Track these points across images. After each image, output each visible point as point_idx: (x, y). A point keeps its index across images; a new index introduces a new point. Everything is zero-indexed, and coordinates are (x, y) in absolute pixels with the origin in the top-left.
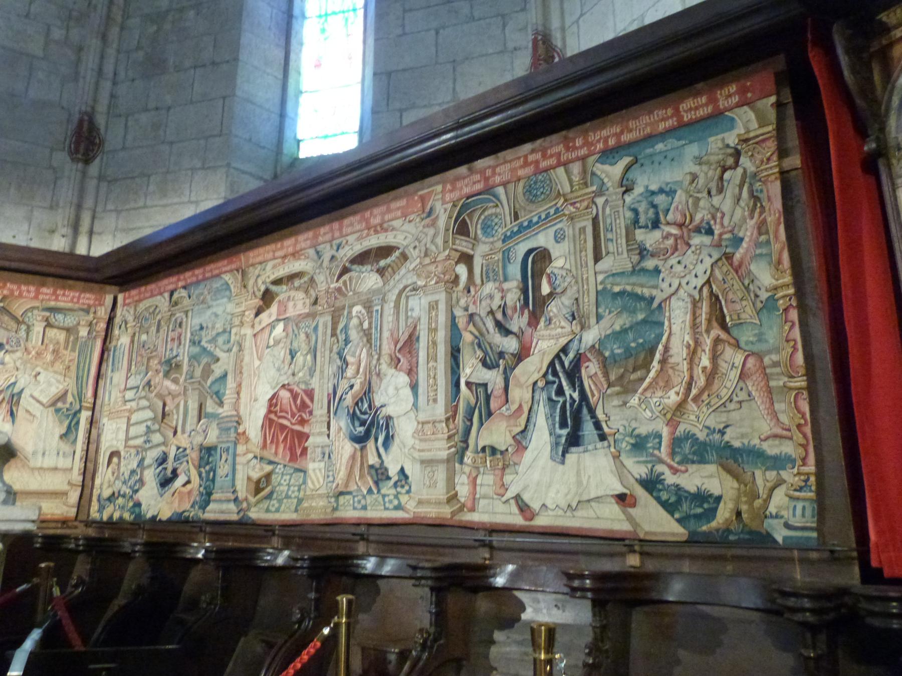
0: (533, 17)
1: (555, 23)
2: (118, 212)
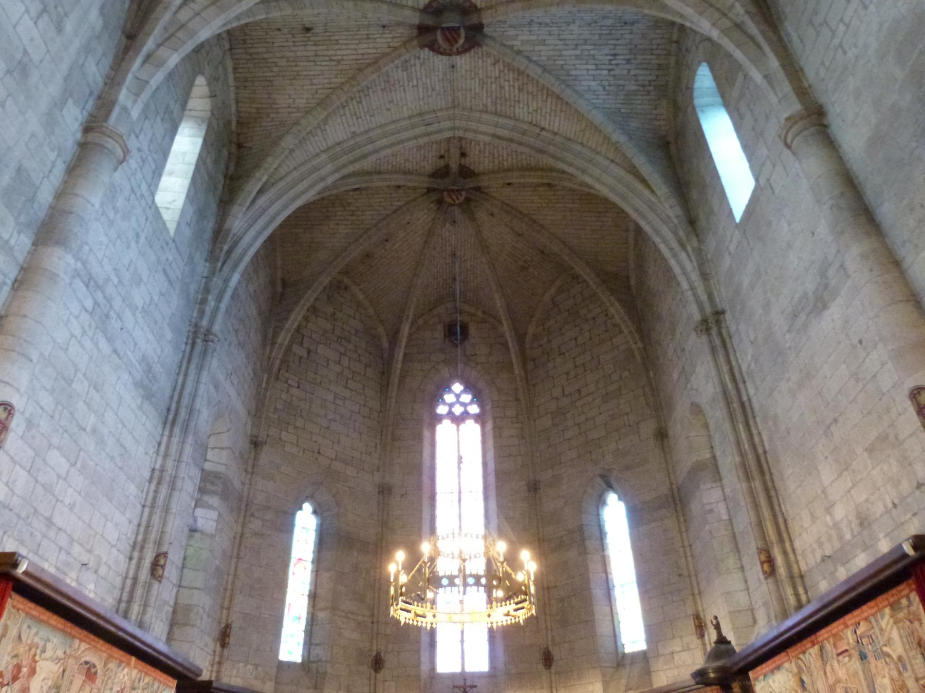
0: (690, 611)
1: (700, 609)
2: (565, 687)
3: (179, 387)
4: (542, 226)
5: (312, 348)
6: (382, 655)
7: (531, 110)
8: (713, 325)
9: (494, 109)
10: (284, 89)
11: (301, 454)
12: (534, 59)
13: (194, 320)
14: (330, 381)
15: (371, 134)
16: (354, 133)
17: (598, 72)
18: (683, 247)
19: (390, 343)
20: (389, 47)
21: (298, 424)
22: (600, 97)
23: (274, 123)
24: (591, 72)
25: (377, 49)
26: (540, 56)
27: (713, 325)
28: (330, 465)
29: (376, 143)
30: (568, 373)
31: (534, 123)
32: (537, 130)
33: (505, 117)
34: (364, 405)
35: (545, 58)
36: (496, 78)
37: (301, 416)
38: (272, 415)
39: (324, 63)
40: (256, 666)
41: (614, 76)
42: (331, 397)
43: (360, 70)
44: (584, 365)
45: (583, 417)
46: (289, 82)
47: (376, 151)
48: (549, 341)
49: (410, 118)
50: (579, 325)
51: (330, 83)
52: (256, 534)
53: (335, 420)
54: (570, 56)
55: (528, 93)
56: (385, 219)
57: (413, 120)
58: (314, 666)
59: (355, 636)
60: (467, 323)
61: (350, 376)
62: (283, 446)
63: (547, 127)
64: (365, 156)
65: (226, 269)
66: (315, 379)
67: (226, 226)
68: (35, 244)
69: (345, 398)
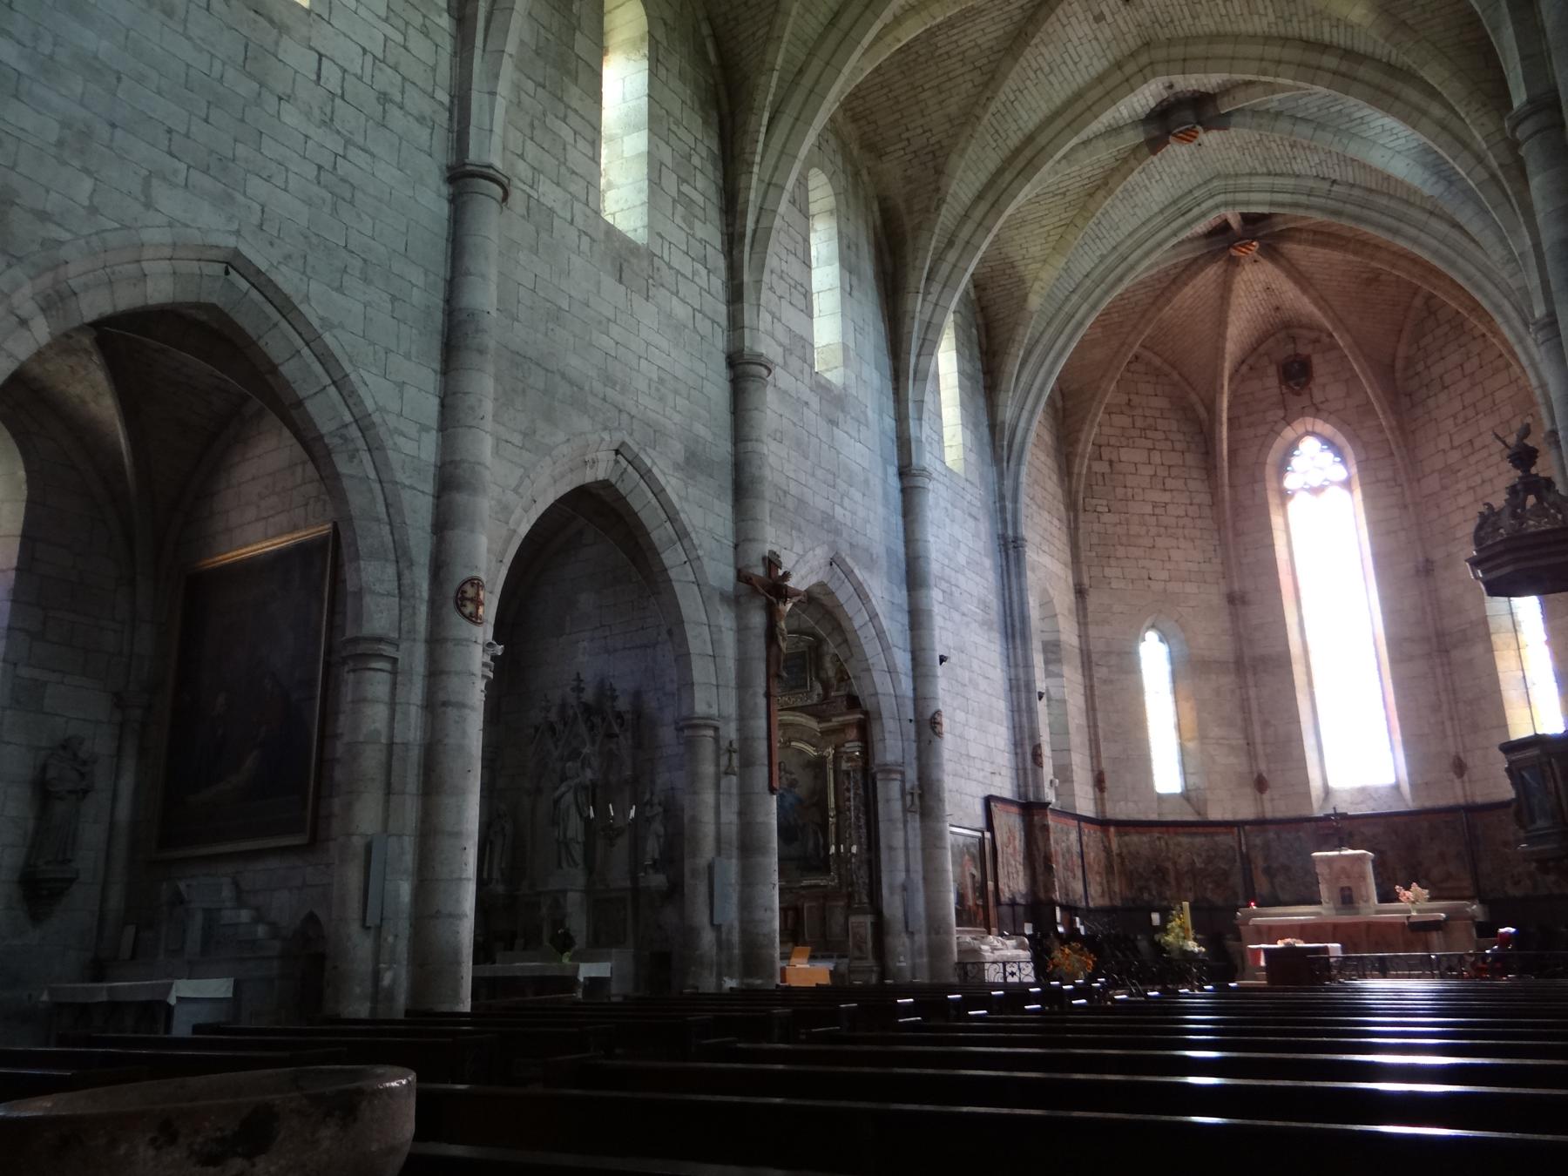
3: (1007, 601)
5: (1114, 458)
6: (1265, 775)
10: (1013, 240)
11: (1130, 586)
13: (1000, 532)
14: (1143, 489)
20: (1117, 160)
21: (1118, 555)
22: (1400, 135)
25: (1103, 167)
26: (1307, 109)
28: (1165, 590)
33: (1282, 175)
34: (1191, 504)
36: (1258, 142)
37: (1122, 545)
38: (1089, 554)
39: (1047, 201)
42: (1148, 509)
43: (1091, 195)
44: (1474, 405)
45: (1478, 479)
46: (1016, 232)
47: (1132, 268)
49: (1161, 211)
50: (1465, 345)
53: (1159, 536)
55: (1304, 149)
58: (1193, 794)
59: (1232, 760)
60: (1309, 357)
62: (1110, 583)
63: (1338, 178)
64: (1120, 279)
65: (1012, 464)
66: (1126, 493)
67: (1000, 418)
68: (909, 590)
69: (1166, 504)
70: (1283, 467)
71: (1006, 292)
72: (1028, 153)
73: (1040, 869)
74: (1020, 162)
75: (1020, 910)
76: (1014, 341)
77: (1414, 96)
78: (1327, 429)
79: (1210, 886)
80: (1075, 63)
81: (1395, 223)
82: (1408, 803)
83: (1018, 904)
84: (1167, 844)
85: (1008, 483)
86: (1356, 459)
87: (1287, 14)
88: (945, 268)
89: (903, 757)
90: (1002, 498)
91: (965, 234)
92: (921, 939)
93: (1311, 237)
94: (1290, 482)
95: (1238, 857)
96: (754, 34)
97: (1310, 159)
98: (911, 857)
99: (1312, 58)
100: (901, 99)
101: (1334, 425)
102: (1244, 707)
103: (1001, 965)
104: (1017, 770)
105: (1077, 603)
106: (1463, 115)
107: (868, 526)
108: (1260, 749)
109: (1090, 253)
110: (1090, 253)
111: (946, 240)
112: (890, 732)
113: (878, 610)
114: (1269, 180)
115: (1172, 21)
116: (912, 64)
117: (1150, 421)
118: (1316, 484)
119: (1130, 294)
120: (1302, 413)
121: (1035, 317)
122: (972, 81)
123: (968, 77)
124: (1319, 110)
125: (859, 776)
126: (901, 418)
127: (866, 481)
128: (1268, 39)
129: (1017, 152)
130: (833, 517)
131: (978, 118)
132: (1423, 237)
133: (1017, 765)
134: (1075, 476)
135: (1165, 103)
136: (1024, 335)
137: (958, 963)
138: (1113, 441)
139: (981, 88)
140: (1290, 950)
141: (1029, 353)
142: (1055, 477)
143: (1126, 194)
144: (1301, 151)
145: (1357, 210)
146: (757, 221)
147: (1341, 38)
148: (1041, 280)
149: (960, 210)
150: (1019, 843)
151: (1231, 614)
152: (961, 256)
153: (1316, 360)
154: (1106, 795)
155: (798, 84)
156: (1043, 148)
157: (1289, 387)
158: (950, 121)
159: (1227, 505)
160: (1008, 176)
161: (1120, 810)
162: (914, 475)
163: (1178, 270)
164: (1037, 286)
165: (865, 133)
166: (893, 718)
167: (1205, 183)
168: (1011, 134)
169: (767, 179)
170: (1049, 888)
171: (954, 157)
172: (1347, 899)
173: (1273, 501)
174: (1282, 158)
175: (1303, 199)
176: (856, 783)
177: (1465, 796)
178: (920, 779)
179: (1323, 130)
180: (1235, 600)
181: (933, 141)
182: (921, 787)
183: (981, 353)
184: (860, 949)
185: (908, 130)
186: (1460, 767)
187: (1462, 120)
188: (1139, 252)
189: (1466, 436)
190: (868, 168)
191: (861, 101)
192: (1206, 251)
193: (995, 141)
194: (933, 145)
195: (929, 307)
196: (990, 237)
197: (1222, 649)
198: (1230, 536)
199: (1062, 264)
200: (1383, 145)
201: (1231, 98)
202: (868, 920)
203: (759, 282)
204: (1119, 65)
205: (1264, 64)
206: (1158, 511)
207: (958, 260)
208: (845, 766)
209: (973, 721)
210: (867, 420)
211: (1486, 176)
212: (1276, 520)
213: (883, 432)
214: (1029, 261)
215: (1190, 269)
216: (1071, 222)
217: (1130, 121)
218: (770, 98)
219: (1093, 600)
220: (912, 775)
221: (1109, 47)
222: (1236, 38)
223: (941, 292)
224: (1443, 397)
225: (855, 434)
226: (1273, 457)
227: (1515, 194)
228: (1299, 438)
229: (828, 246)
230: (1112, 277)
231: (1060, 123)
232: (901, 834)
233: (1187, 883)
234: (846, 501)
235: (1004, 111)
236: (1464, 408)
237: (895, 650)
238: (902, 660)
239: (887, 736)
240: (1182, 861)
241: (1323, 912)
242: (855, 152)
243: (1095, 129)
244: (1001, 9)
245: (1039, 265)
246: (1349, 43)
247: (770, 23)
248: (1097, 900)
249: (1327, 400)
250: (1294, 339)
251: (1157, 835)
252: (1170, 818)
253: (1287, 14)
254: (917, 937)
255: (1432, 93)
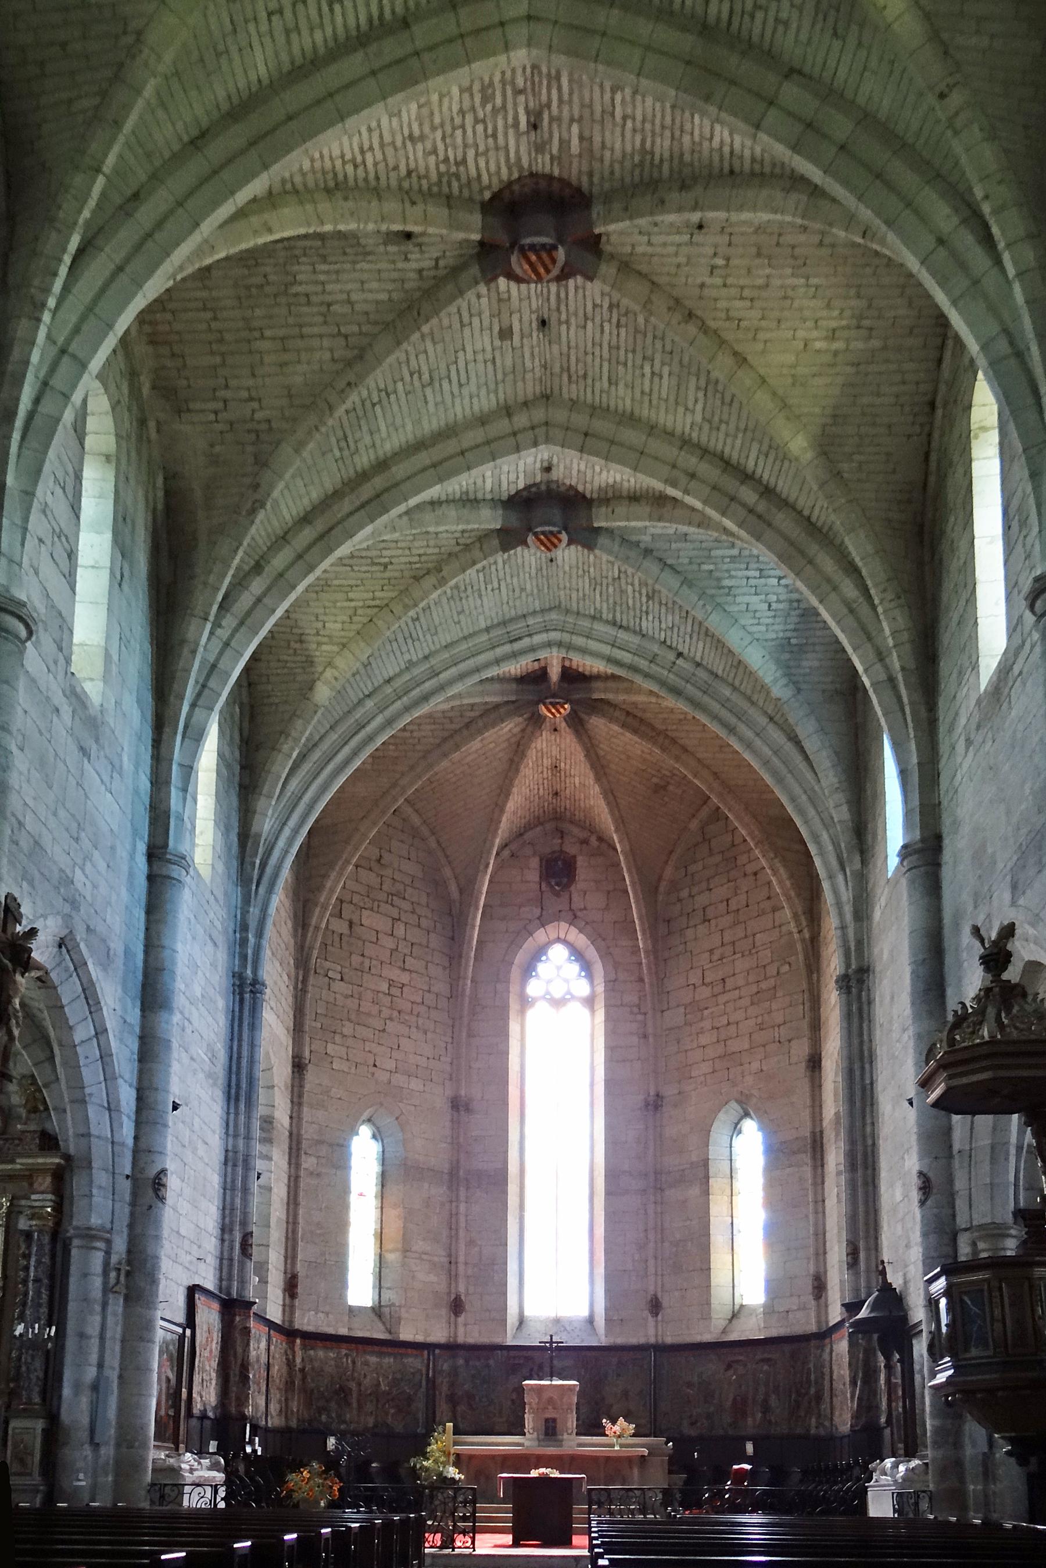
3: (235, 1056)
4: (685, 750)
5: (355, 919)
7: (663, 626)
8: (853, 983)
9: (611, 616)
12: (669, 562)
15: (433, 661)
16: (410, 661)
17: (763, 581)
18: (843, 869)
19: (461, 891)
20: (458, 544)
21: (345, 1031)
23: (298, 658)
24: (752, 582)
27: (853, 983)
29: (441, 676)
30: (711, 951)
31: (668, 643)
32: (671, 656)
33: (626, 629)
35: (686, 561)
36: (614, 579)
37: (349, 1020)
38: (314, 1024)
40: (327, 1314)
41: (787, 586)
42: (384, 987)
43: (417, 579)
48: (691, 896)
49: (487, 630)
51: (374, 599)
52: (312, 1173)
53: (391, 1019)
54: (723, 557)
56: (451, 736)
57: (494, 633)
58: (386, 1310)
59: (432, 1278)
61: (407, 951)
63: (686, 652)
64: (425, 698)
65: (262, 890)
66: (362, 963)
67: (255, 829)
70: (528, 970)
71: (286, 671)
72: (378, 482)
73: (234, 1378)
74: (366, 491)
75: (207, 1424)
76: (288, 735)
77: (828, 564)
78: (581, 940)
79: (392, 1411)
80: (461, 385)
81: (733, 720)
82: (601, 1338)
83: (209, 1418)
84: (354, 1362)
85: (254, 911)
86: (605, 977)
87: (716, 419)
88: (245, 601)
89: (112, 1222)
90: (244, 927)
91: (279, 561)
92: (108, 1452)
93: (623, 718)
94: (533, 988)
95: (424, 1383)
96: (70, 101)
97: (663, 619)
98: (108, 1353)
99: (730, 483)
100: (228, 337)
101: (588, 937)
102: (452, 1224)
103: (209, 1489)
104: (221, 1259)
105: (293, 1078)
106: (876, 601)
107: (109, 909)
108: (461, 1268)
109: (398, 654)
110: (398, 654)
111: (252, 563)
112: (100, 1187)
113: (108, 1026)
114: (612, 631)
115: (585, 376)
116: (254, 290)
117: (400, 887)
118: (558, 994)
119: (416, 727)
120: (557, 917)
121: (319, 714)
122: (331, 350)
123: (326, 343)
124: (691, 563)
125: (46, 1239)
126: (159, 781)
127: (113, 848)
128: (685, 443)
129: (363, 477)
130: (72, 882)
131: (331, 408)
132: (758, 742)
133: (222, 1253)
134: (311, 929)
135: (534, 489)
136: (302, 733)
137: (153, 1485)
138: (356, 899)
139: (340, 366)
140: (544, 1480)
141: (303, 757)
142: (290, 924)
143: (455, 592)
144: (657, 606)
145: (698, 694)
146: (37, 401)
147: (766, 473)
148: (336, 668)
149: (277, 527)
150: (215, 1346)
151: (452, 1121)
152: (269, 589)
153: (581, 861)
154: (297, 1302)
155: (129, 215)
156: (396, 485)
157: (549, 883)
158: (290, 396)
159: (467, 1000)
160: (346, 505)
161: (307, 1321)
162: (169, 861)
163: (472, 714)
164: (329, 673)
165: (163, 368)
166: (106, 1170)
167: (542, 611)
168: (362, 450)
169: (61, 340)
170: (242, 1400)
171: (286, 449)
172: (550, 1430)
173: (514, 1006)
174: (634, 609)
175: (643, 664)
176: (40, 1247)
177: (656, 1336)
178: (129, 1252)
179: (690, 587)
180: (458, 1105)
181: (259, 415)
182: (129, 1262)
183: (242, 740)
184: (22, 1462)
185: (227, 387)
186: (655, 1306)
187: (874, 608)
188: (453, 671)
189: (720, 975)
190: (158, 423)
191: (169, 316)
192: (513, 698)
193: (341, 449)
194: (259, 422)
195: (216, 646)
196: (310, 579)
197: (439, 1158)
198: (464, 1034)
199: (364, 658)
200: (744, 627)
201: (610, 509)
202: (39, 1425)
203: (29, 494)
204: (507, 411)
205: (675, 472)
206: (395, 991)
207: (264, 594)
208: (23, 1224)
209: (187, 1191)
210: (121, 767)
211: (883, 677)
212: (514, 1027)
213: (136, 791)
214: (325, 640)
215: (491, 714)
216: (387, 605)
217: (489, 496)
218: (86, 214)
219: (311, 1076)
220: (120, 1245)
221: (503, 381)
222: (652, 429)
223: (236, 630)
224: (702, 929)
225: (106, 778)
226: (521, 957)
227: (911, 703)
228: (549, 944)
229: (97, 504)
230: (416, 693)
231: (424, 458)
232: (98, 1319)
233: (369, 1407)
234: (88, 866)
235: (360, 413)
236: (723, 945)
237: (120, 1081)
238: (127, 1096)
239: (95, 1191)
240: (367, 1382)
241: (527, 1443)
242: (146, 390)
243: (450, 490)
244: (394, 262)
245: (335, 648)
246: (773, 481)
247: (104, 94)
248: (275, 1421)
249: (585, 909)
250: (562, 834)
251: (344, 1352)
252: (360, 1334)
253: (716, 419)
254: (103, 1451)
255: (852, 570)
